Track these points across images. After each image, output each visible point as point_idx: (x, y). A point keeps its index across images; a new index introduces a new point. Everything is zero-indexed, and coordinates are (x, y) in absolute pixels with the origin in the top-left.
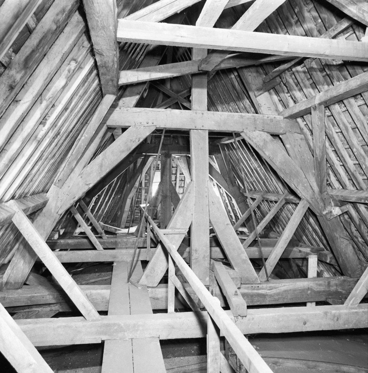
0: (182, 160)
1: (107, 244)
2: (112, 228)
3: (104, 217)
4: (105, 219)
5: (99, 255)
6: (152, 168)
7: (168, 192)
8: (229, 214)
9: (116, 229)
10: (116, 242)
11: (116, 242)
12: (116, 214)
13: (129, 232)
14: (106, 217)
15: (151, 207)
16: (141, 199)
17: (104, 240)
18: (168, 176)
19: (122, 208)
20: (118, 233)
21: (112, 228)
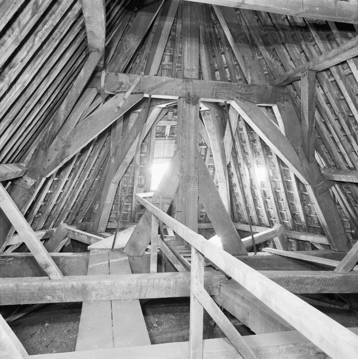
0: (210, 116)
1: (59, 293)
2: (83, 236)
3: (70, 213)
4: (72, 216)
5: (56, 286)
6: (154, 132)
7: (193, 169)
8: (279, 211)
9: (90, 238)
10: (84, 287)
11: (84, 287)
12: (91, 209)
13: (115, 247)
14: (73, 214)
15: (159, 198)
16: (133, 185)
17: (53, 284)
18: (192, 140)
19: (99, 198)
20: (94, 249)
21: (82, 234)
